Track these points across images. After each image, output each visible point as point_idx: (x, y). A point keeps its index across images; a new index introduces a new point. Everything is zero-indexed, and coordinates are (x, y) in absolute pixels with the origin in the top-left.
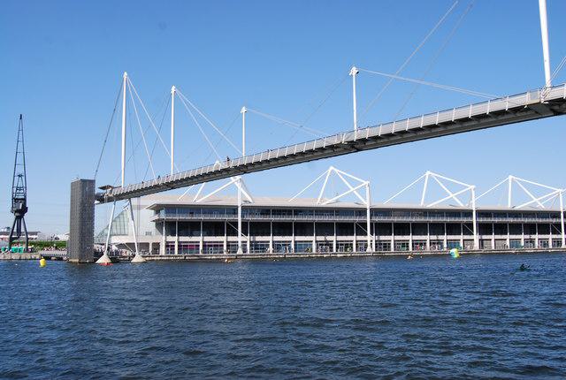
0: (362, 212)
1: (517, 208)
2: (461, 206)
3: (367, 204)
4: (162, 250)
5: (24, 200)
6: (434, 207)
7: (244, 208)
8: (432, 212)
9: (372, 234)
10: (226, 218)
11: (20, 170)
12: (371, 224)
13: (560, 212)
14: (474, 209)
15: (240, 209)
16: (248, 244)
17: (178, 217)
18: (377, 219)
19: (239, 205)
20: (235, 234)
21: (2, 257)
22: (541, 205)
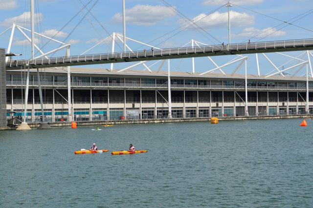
8: (215, 81)
19: (246, 78)
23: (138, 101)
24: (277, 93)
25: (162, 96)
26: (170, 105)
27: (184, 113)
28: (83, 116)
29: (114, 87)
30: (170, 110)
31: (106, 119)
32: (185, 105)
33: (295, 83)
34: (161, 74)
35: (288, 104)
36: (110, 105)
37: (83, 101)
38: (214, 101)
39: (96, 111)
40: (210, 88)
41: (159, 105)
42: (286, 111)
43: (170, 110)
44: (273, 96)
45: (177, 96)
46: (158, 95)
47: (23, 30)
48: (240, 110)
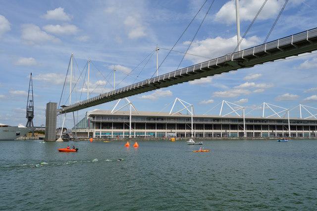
0: (189, 119)
1: (267, 118)
2: (239, 116)
3: (192, 115)
4: (94, 135)
5: (33, 112)
6: (226, 117)
7: (133, 117)
8: (223, 119)
9: (194, 129)
10: (124, 121)
11: (31, 99)
12: (194, 125)
13: (287, 120)
14: (289, 119)
15: (130, 117)
16: (143, 135)
17: (101, 121)
18: (248, 123)
19: (192, 116)
20: (128, 128)
21: (316, 131)
22: (280, 117)
23: (275, 129)
24: (123, 123)
25: (286, 128)
26: (290, 131)
27: (297, 135)
28: (141, 135)
29: (160, 122)
30: (290, 134)
31: (155, 137)
32: (297, 132)
33: (122, 117)
34: (285, 118)
35: (276, 131)
36: (156, 131)
37: (294, 130)
38: (311, 130)
39: (149, 133)
40: (309, 124)
41: (285, 131)
42: (275, 135)
43: (290, 134)
44: (306, 128)
45: (293, 128)
46: (187, 126)
47: (228, 103)
48: (287, 135)
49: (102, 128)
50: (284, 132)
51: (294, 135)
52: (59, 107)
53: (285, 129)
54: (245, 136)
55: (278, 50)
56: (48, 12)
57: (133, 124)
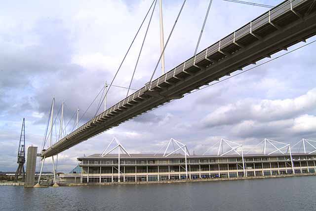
9: (188, 170)
10: (179, 163)
12: (188, 166)
13: (118, 154)
24: (146, 167)
26: (293, 168)
32: (301, 168)
45: (297, 164)
48: (241, 174)
49: (137, 172)
50: (286, 169)
51: (297, 171)
52: (39, 151)
53: (288, 166)
54: (246, 175)
55: (209, 63)
56: (287, 48)
57: (122, 168)
